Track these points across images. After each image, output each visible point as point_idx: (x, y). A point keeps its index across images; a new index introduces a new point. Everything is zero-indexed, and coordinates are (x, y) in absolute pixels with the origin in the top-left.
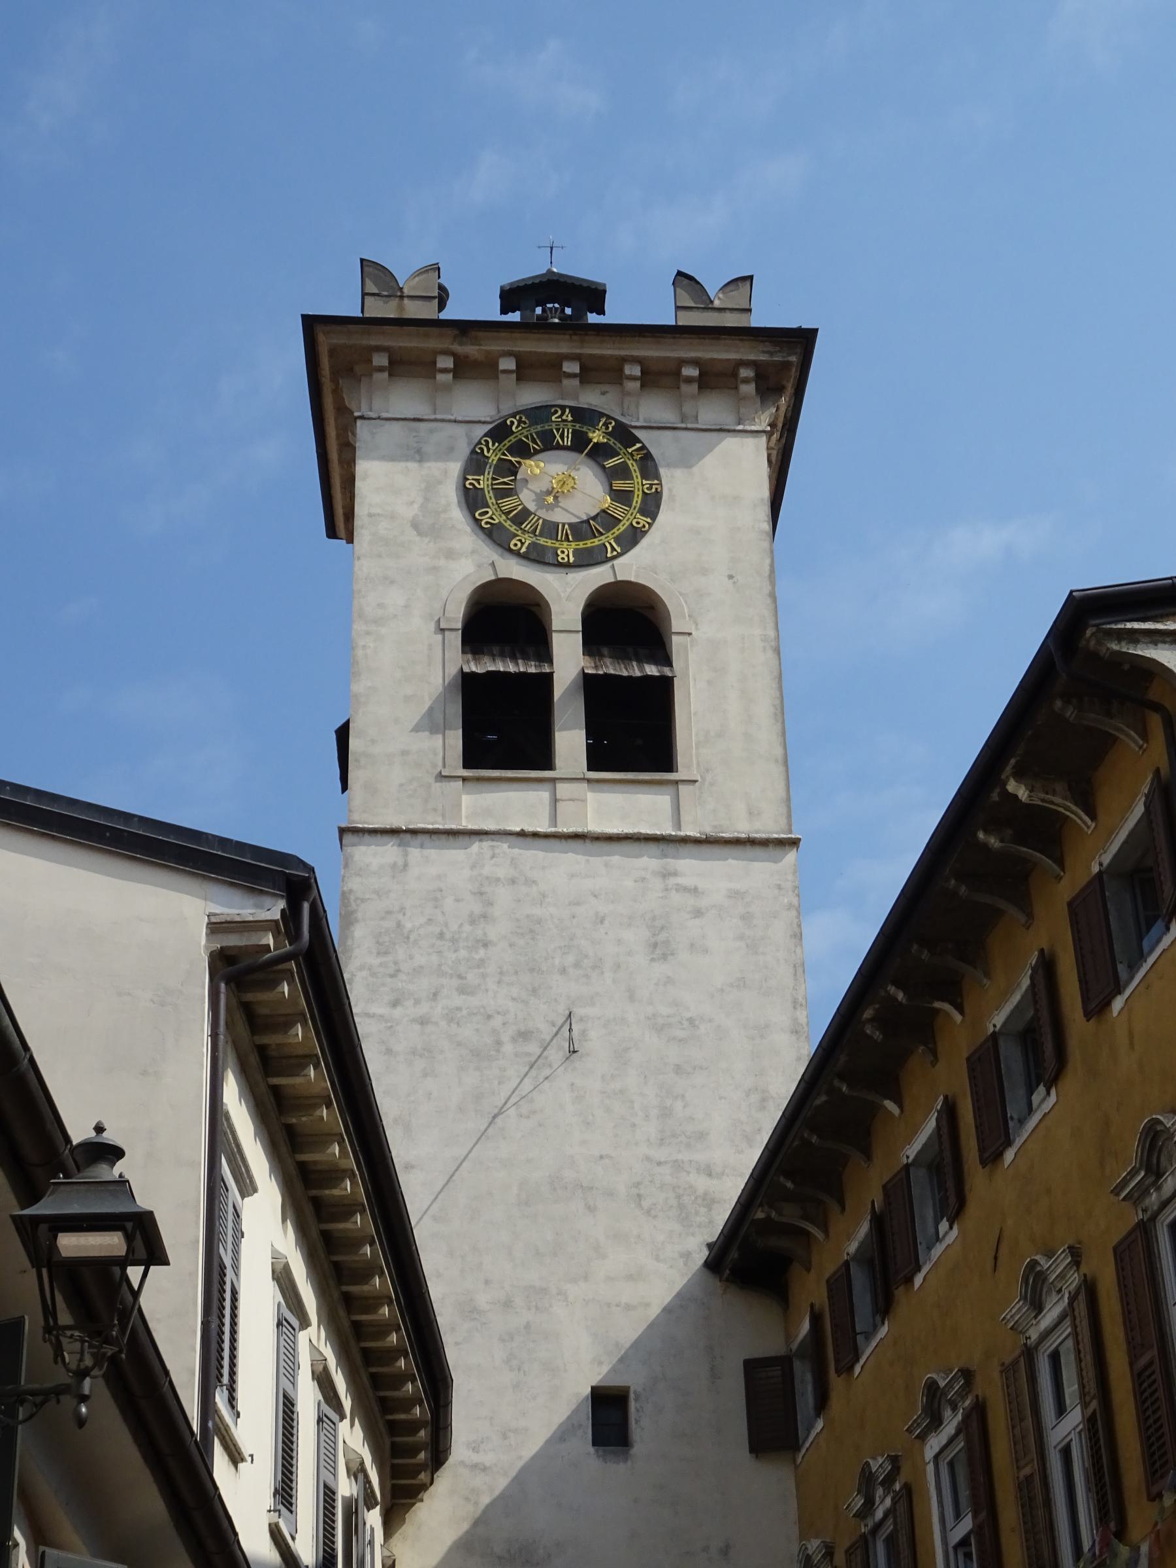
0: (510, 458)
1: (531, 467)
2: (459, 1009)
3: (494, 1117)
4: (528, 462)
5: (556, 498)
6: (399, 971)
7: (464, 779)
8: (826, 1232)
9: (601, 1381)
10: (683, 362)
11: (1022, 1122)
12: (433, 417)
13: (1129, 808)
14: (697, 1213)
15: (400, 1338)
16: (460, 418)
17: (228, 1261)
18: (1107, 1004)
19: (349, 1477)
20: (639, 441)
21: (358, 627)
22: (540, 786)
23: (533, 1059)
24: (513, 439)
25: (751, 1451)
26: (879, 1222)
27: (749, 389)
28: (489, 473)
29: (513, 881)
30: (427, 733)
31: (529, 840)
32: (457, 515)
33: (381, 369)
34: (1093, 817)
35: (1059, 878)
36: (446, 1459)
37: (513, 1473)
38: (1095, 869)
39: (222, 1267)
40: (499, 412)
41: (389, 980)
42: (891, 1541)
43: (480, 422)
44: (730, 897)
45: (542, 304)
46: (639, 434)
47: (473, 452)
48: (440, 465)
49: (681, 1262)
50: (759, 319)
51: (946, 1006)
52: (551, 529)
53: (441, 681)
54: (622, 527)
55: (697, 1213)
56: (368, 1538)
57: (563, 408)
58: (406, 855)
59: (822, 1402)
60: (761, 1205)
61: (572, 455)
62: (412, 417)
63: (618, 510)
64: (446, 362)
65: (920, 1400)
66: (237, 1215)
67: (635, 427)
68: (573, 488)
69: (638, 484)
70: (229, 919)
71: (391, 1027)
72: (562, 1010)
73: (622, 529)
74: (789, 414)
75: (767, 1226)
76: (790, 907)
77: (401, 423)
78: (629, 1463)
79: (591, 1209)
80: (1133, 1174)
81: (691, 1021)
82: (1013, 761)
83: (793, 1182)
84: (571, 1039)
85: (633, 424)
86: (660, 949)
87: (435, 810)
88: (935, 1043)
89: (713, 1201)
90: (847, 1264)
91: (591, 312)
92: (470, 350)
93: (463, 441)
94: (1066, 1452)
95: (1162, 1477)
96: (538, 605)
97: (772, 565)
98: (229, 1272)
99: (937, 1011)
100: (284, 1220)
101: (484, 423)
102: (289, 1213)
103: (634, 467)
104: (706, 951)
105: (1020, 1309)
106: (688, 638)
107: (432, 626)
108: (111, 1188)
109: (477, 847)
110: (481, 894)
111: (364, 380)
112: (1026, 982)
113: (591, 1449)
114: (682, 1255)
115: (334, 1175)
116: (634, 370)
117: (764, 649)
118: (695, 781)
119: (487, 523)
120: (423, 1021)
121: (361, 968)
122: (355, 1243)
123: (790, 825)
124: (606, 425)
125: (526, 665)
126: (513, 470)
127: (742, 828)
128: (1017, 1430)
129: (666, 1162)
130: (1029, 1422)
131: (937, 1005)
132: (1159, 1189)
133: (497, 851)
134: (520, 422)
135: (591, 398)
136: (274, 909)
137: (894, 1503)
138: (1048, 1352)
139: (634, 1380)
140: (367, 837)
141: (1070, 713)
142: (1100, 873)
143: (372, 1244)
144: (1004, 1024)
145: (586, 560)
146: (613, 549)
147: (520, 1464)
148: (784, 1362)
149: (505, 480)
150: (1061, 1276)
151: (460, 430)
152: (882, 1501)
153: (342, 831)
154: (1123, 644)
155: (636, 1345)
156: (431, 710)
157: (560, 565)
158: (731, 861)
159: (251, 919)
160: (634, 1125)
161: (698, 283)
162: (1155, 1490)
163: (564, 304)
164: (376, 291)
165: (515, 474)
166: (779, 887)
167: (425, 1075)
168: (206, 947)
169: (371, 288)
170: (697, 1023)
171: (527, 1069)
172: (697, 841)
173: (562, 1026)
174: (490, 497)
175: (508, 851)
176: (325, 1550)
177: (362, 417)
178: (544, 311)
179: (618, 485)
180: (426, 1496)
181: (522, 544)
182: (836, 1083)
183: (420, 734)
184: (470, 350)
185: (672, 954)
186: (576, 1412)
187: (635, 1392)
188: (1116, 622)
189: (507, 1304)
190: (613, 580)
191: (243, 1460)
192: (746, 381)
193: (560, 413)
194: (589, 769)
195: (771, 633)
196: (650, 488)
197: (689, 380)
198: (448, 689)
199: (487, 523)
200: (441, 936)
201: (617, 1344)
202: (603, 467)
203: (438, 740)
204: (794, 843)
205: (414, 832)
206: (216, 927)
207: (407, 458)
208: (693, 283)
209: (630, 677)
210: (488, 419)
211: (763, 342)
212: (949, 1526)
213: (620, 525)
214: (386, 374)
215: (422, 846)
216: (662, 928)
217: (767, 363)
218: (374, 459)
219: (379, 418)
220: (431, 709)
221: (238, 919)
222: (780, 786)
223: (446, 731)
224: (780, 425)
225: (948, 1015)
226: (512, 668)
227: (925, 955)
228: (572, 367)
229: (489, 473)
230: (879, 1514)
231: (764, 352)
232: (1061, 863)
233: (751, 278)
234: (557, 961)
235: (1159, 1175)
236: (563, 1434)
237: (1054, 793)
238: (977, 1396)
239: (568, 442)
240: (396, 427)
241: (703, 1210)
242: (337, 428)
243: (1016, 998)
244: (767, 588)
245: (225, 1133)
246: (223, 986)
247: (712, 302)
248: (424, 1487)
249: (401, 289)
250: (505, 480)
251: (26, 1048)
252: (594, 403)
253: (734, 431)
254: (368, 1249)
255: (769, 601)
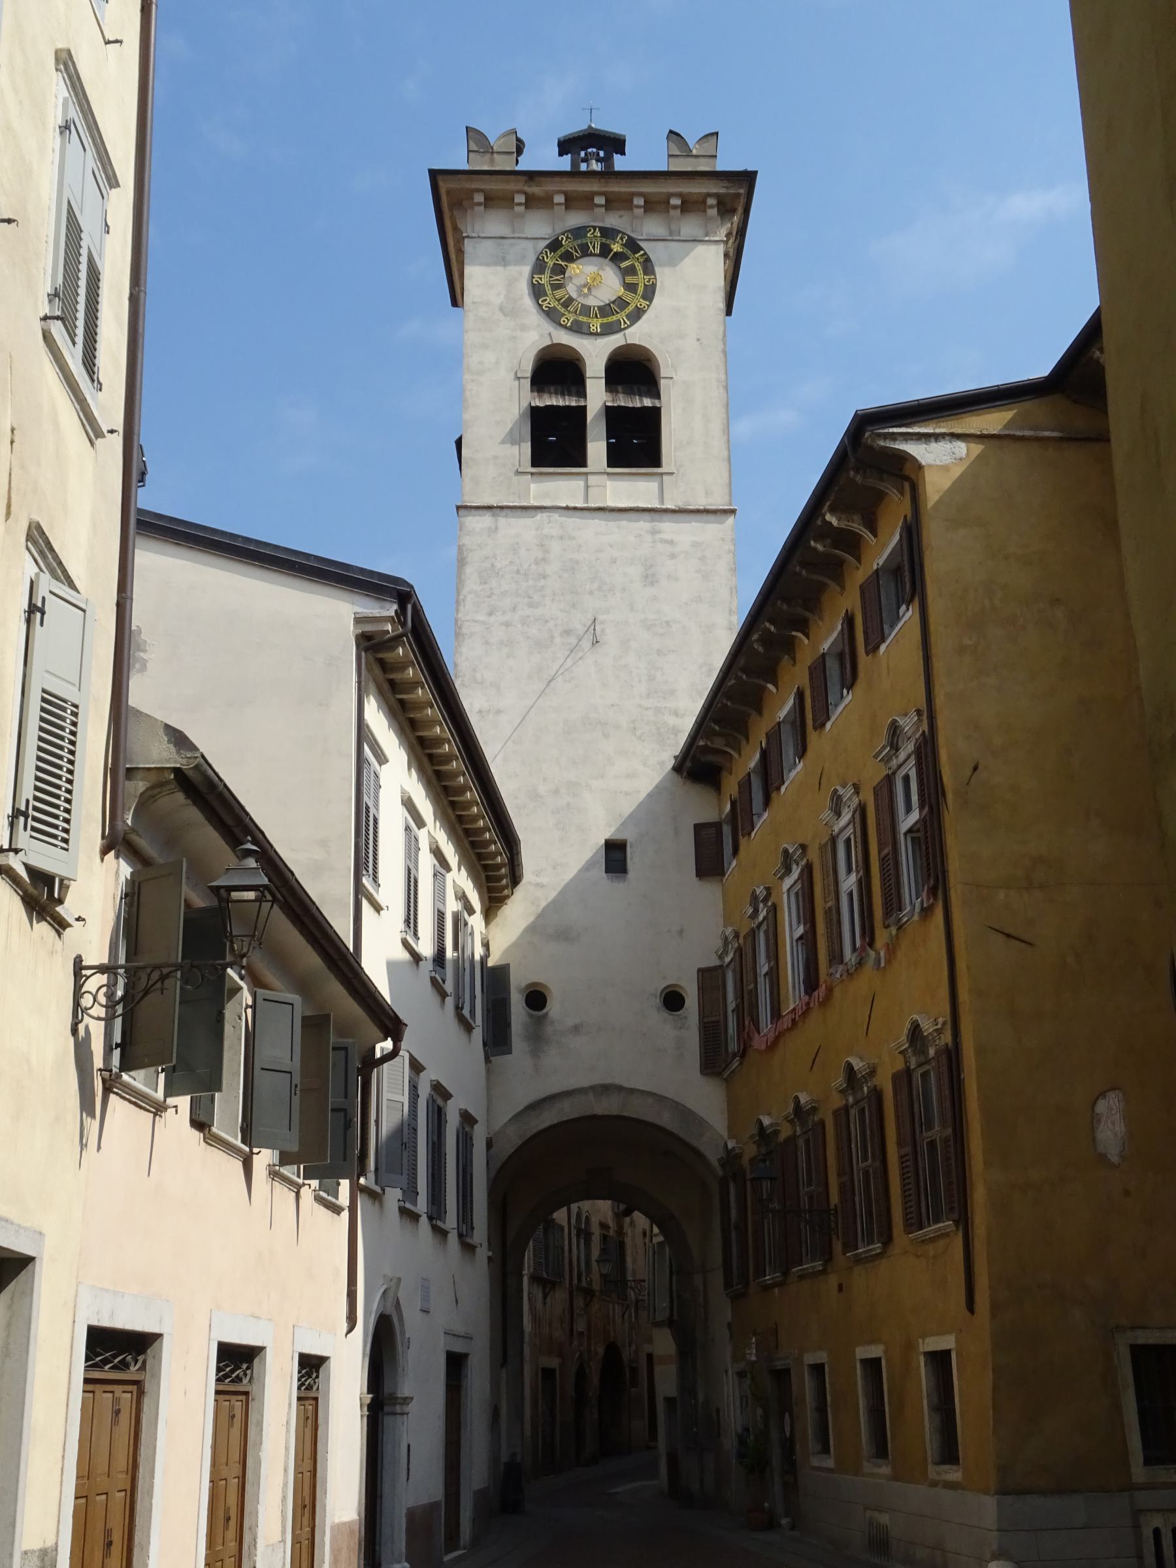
0: (561, 262)
1: (574, 269)
2: (528, 617)
3: (550, 682)
4: (573, 265)
5: (589, 289)
6: (493, 594)
7: (532, 474)
8: (740, 754)
9: (612, 835)
10: (671, 195)
11: (836, 706)
12: (512, 236)
13: (892, 534)
14: (668, 738)
15: (485, 822)
16: (529, 236)
17: (370, 804)
18: (877, 648)
19: (456, 900)
20: (643, 250)
21: (467, 377)
22: (578, 477)
23: (573, 647)
24: (562, 250)
25: (697, 876)
26: (764, 754)
27: (713, 212)
28: (548, 272)
29: (561, 538)
30: (509, 445)
31: (571, 512)
32: (528, 302)
33: (479, 204)
34: (875, 536)
35: (858, 568)
36: (520, 881)
37: (559, 889)
38: (875, 567)
39: (367, 808)
40: (554, 230)
41: (487, 599)
42: (766, 932)
43: (542, 238)
44: (692, 546)
45: (585, 149)
46: (642, 244)
47: (538, 259)
48: (517, 268)
49: (658, 767)
50: (721, 165)
51: (799, 635)
52: (586, 310)
53: (518, 411)
54: (631, 308)
55: (668, 738)
56: (469, 931)
57: (595, 228)
58: (496, 522)
59: (736, 851)
60: (702, 738)
61: (601, 260)
62: (499, 236)
63: (628, 297)
64: (519, 198)
65: (780, 859)
66: (377, 776)
67: (640, 240)
68: (600, 282)
69: (641, 279)
70: (366, 615)
71: (488, 628)
72: (590, 617)
73: (631, 309)
74: (740, 226)
75: (705, 750)
76: (729, 551)
77: (492, 240)
78: (626, 883)
79: (606, 736)
80: (884, 748)
81: (667, 623)
82: (828, 504)
83: (719, 727)
84: (594, 634)
85: (639, 238)
86: (650, 579)
87: (514, 493)
88: (794, 654)
89: (678, 731)
90: (749, 774)
91: (617, 153)
92: (535, 190)
93: (531, 251)
94: (851, 894)
95: (890, 916)
96: (578, 360)
97: (724, 332)
98: (372, 811)
99: (795, 637)
100: (409, 769)
101: (545, 239)
102: (414, 764)
103: (639, 267)
104: (677, 579)
105: (829, 815)
106: (671, 381)
107: (512, 376)
108: (253, 871)
109: (540, 516)
110: (542, 546)
111: (469, 211)
112: (839, 627)
113: (604, 875)
114: (659, 763)
115: (438, 742)
116: (639, 201)
117: (718, 386)
118: (673, 473)
119: (546, 307)
120: (507, 624)
121: (470, 592)
122: (455, 775)
123: (730, 500)
124: (622, 239)
125: (570, 400)
126: (562, 271)
127: (701, 502)
128: (826, 881)
129: (651, 708)
130: (831, 878)
131: (794, 633)
132: (897, 757)
133: (552, 519)
134: (567, 238)
135: (613, 220)
136: (391, 609)
137: (767, 913)
138: (845, 838)
139: (629, 836)
140: (473, 511)
141: (859, 479)
142: (877, 570)
143: (464, 775)
144: (829, 648)
145: (609, 330)
146: (625, 322)
147: (563, 884)
148: (717, 826)
149: (558, 278)
150: (850, 799)
151: (529, 245)
152: (762, 911)
153: (458, 508)
154: (887, 441)
155: (631, 816)
156: (512, 430)
157: (591, 334)
158: (694, 524)
159: (378, 615)
160: (632, 686)
161: (682, 138)
162: (887, 923)
163: (599, 149)
164: (476, 149)
165: (564, 273)
166: (723, 540)
167: (508, 657)
168: (353, 631)
169: (473, 147)
170: (671, 624)
171: (568, 653)
172: (673, 511)
173: (590, 626)
174: (548, 289)
175: (558, 518)
176: (438, 946)
177: (468, 237)
178: (586, 154)
179: (629, 279)
180: (509, 902)
181: (568, 320)
182: (739, 674)
183: (505, 446)
184: (535, 190)
185: (657, 582)
186: (595, 854)
187: (630, 842)
188: (884, 428)
189: (556, 792)
190: (624, 343)
191: (382, 909)
192: (711, 207)
193: (592, 231)
194: (608, 466)
195: (723, 377)
196: (649, 281)
197: (675, 207)
198: (522, 416)
199: (546, 307)
200: (518, 572)
201: (620, 815)
202: (619, 267)
203: (515, 450)
204: (733, 512)
205: (502, 508)
206: (359, 620)
207: (496, 264)
208: (679, 138)
209: (634, 408)
210: (547, 236)
211: (722, 180)
212: (794, 928)
213: (630, 307)
214: (482, 207)
215: (506, 516)
216: (651, 566)
217: (725, 195)
218: (476, 265)
219: (479, 237)
220: (512, 429)
221: (371, 615)
222: (726, 475)
223: (522, 444)
224: (734, 233)
225: (801, 639)
226: (561, 403)
227: (785, 607)
228: (600, 200)
229: (548, 272)
230: (761, 918)
231: (723, 187)
232: (859, 560)
233: (717, 133)
234: (588, 587)
235: (897, 750)
236: (589, 866)
237: (853, 522)
238: (808, 860)
239: (597, 251)
240: (489, 243)
241: (672, 736)
242: (454, 240)
243: (835, 635)
244: (721, 347)
245: (368, 735)
246: (363, 653)
247: (691, 151)
248: (508, 897)
249: (492, 148)
250: (558, 278)
251: (221, 780)
252: (614, 223)
253: (703, 241)
254: (462, 779)
255: (722, 355)
